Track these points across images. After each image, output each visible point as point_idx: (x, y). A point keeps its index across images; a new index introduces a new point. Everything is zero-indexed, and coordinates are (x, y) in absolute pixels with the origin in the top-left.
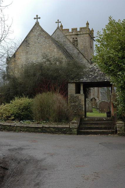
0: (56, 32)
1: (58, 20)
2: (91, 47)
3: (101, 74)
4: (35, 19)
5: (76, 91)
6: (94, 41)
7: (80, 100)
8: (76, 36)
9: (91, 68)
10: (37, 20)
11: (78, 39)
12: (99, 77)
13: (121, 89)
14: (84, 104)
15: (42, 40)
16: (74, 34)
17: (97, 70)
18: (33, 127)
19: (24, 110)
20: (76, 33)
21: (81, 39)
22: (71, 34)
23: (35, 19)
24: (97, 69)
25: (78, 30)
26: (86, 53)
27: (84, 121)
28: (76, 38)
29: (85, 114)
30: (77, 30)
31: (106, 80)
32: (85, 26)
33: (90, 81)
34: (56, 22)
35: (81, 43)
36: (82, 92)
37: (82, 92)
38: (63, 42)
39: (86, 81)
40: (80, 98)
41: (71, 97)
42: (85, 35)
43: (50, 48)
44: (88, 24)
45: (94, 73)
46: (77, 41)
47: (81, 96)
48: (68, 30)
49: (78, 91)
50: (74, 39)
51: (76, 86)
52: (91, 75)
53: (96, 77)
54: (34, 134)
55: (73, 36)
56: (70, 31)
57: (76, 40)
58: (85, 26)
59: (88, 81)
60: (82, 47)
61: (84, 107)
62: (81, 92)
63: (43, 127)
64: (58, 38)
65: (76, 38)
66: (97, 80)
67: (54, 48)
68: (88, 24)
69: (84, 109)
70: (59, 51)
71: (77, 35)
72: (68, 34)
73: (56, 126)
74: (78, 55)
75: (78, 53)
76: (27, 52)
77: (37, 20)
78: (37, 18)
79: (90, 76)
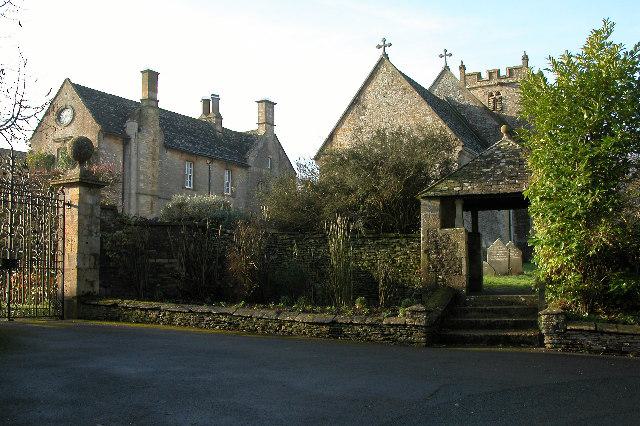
1: (384, 40)
4: (379, 47)
8: (498, 88)
9: (489, 156)
15: (394, 97)
19: (618, 302)
23: (379, 47)
25: (503, 73)
27: (465, 304)
32: (519, 63)
34: (441, 56)
44: (526, 58)
48: (479, 75)
49: (447, 221)
51: (484, 209)
56: (485, 76)
58: (519, 63)
68: (526, 58)
71: (502, 84)
78: (446, 54)
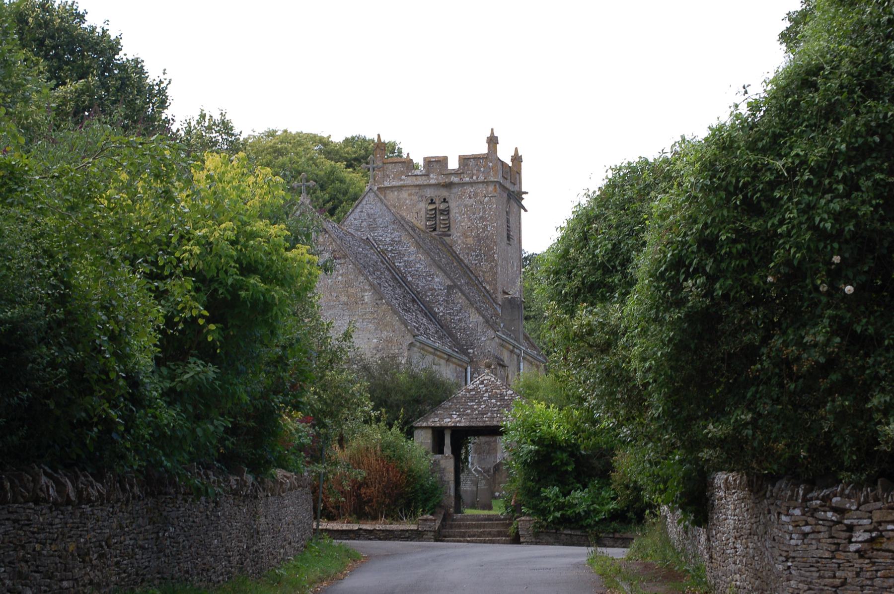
2: (509, 238)
6: (522, 211)
7: (444, 469)
8: (444, 193)
11: (453, 205)
12: (489, 414)
13: (872, 265)
14: (453, 478)
16: (432, 182)
20: (442, 180)
21: (466, 206)
22: (420, 181)
26: (485, 266)
28: (445, 201)
29: (456, 503)
30: (447, 164)
32: (483, 149)
33: (467, 424)
35: (466, 223)
36: (448, 450)
37: (448, 450)
38: (392, 245)
42: (481, 189)
43: (351, 290)
44: (493, 141)
45: (479, 403)
46: (447, 212)
47: (447, 462)
49: (438, 448)
50: (432, 202)
52: (471, 407)
53: (483, 413)
54: (547, 547)
55: (430, 193)
57: (442, 207)
58: (483, 149)
59: (462, 425)
60: (470, 241)
61: (452, 485)
62: (445, 449)
63: (360, 529)
64: (372, 228)
65: (445, 201)
66: (484, 421)
67: (366, 291)
68: (493, 141)
69: (452, 493)
70: (379, 302)
71: (449, 186)
72: (409, 181)
73: (388, 527)
74: (448, 295)
75: (449, 288)
79: (469, 411)
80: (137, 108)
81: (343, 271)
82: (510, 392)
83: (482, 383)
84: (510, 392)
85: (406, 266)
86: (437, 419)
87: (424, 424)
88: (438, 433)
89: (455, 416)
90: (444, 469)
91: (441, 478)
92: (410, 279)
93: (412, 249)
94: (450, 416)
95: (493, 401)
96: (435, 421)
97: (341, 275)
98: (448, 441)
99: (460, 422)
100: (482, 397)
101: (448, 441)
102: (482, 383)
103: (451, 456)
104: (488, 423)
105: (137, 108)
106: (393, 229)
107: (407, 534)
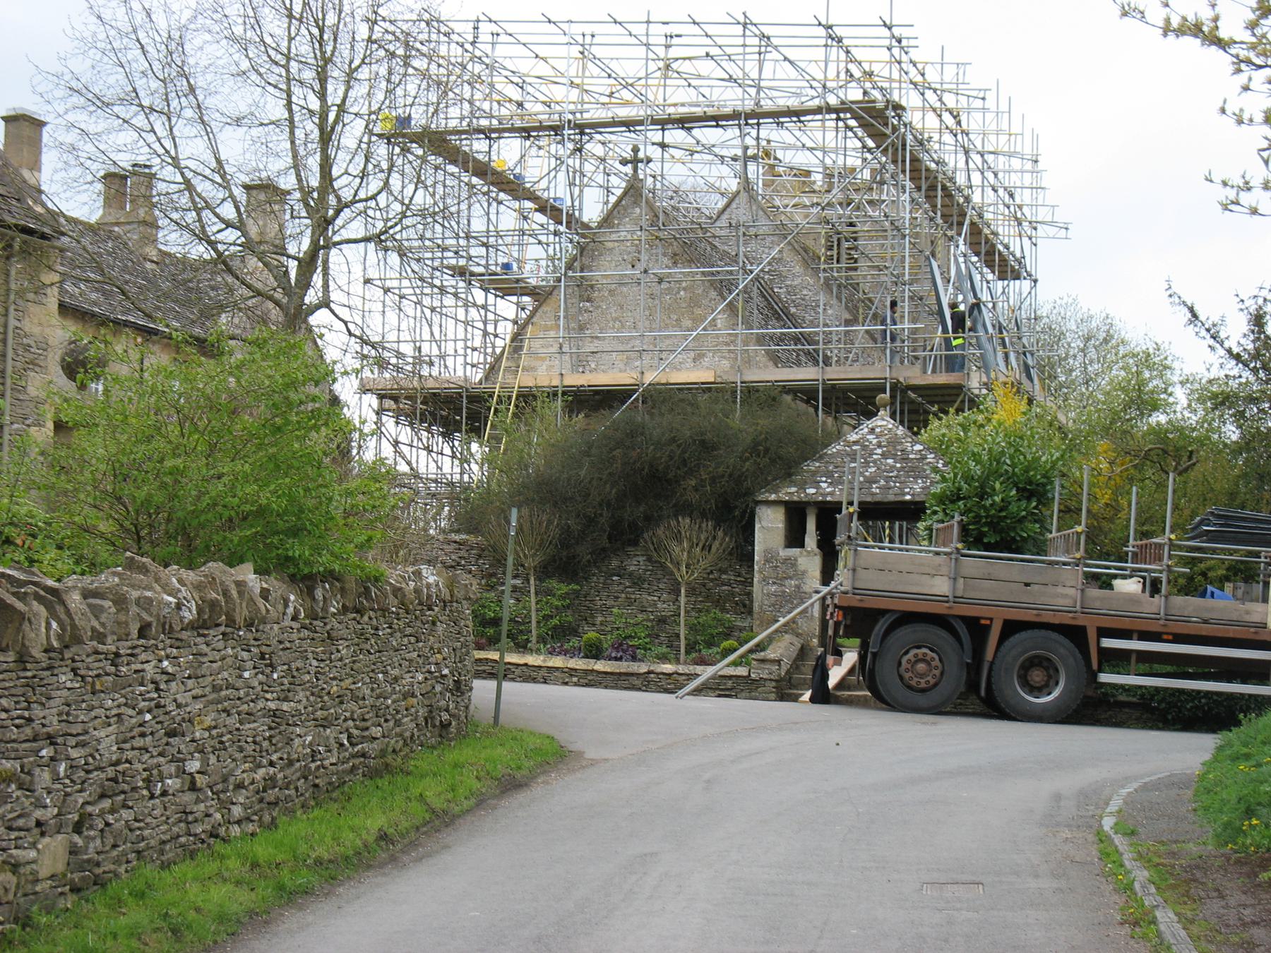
0: (734, 205)
3: (892, 468)
5: (786, 537)
7: (804, 573)
9: (855, 443)
10: (635, 170)
17: (879, 451)
18: (612, 674)
24: (879, 446)
31: (908, 497)
36: (811, 540)
37: (811, 540)
39: (829, 499)
40: (801, 568)
41: (767, 561)
49: (795, 538)
53: (871, 481)
62: (807, 539)
63: (649, 672)
76: (582, 328)
77: (635, 170)
80: (445, 593)
81: (745, 371)
82: (918, 447)
83: (872, 431)
84: (918, 447)
85: (789, 293)
86: (793, 489)
87: (773, 497)
88: (795, 514)
89: (824, 485)
90: (804, 573)
91: (798, 587)
92: (793, 310)
93: (798, 269)
94: (816, 484)
95: (890, 461)
96: (790, 492)
97: (684, 289)
98: (811, 525)
99: (831, 494)
100: (871, 455)
101: (811, 525)
102: (872, 431)
103: (817, 551)
104: (878, 498)
105: (445, 593)
106: (772, 242)
107: (730, 684)
